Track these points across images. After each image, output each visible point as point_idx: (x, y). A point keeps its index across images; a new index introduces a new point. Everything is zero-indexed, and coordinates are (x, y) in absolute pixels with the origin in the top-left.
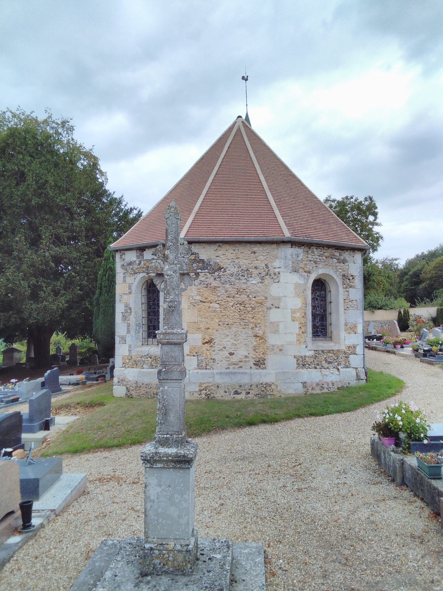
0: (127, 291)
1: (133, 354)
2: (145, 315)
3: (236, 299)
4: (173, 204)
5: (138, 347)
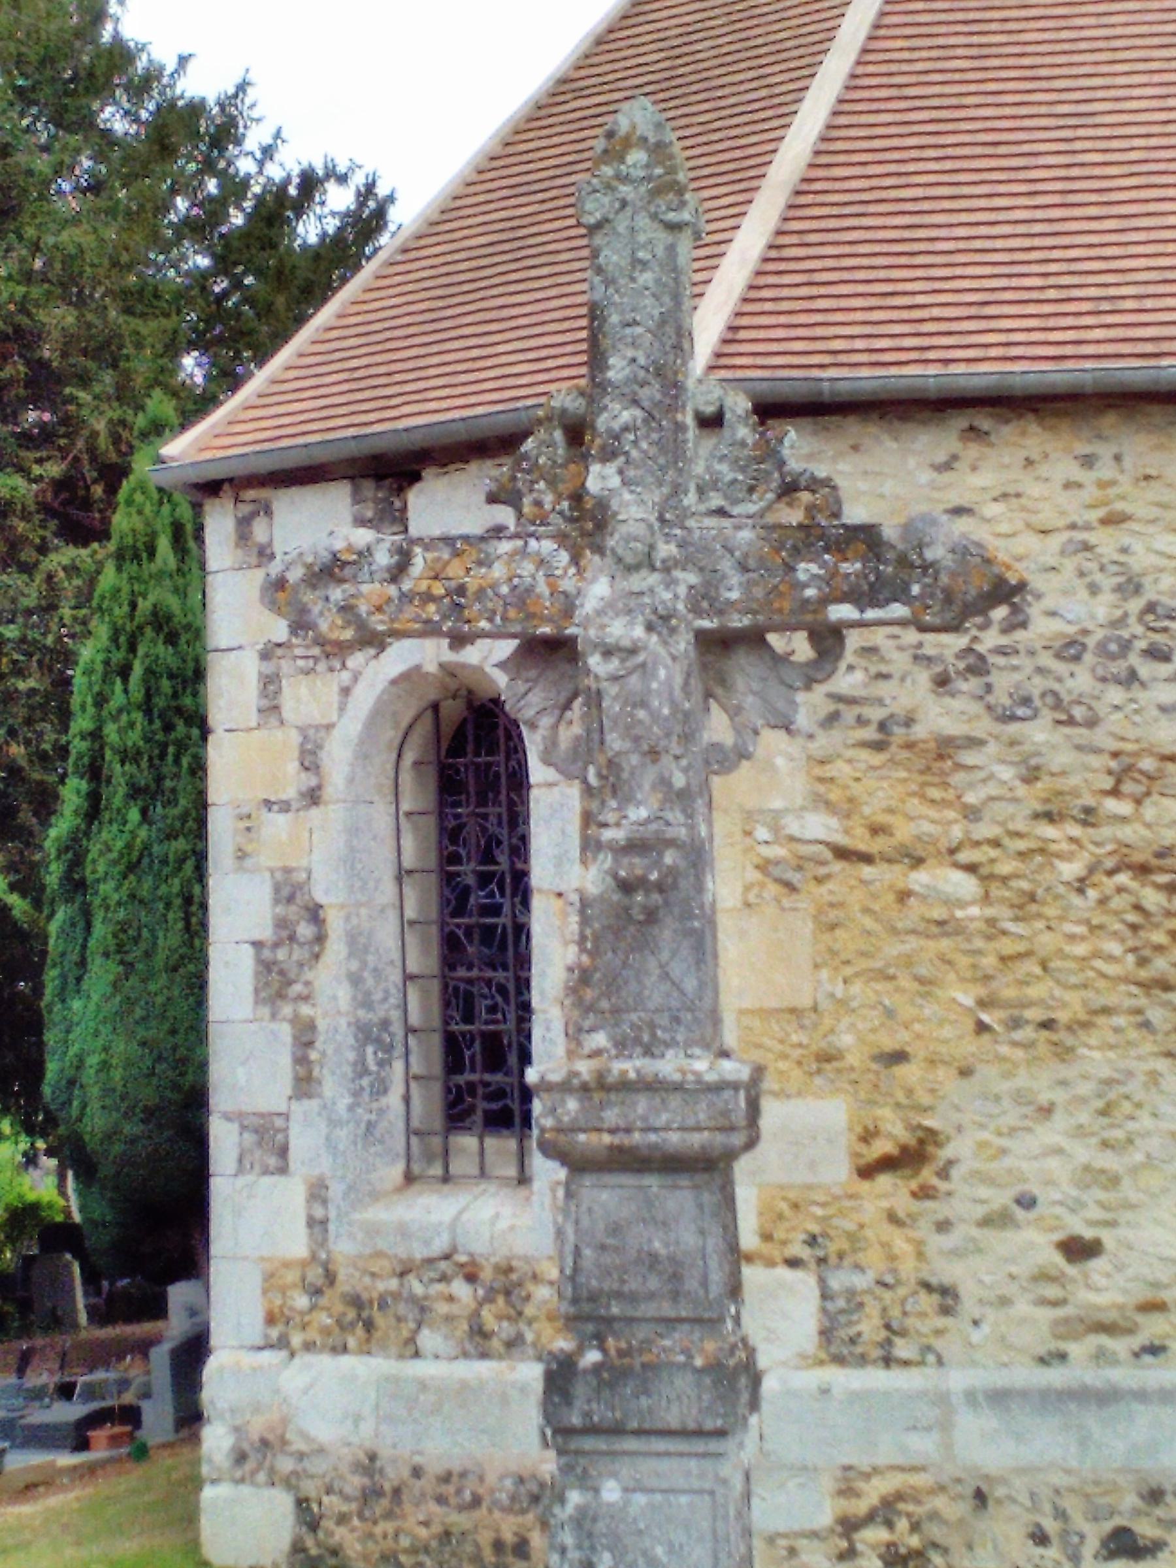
0: (292, 783)
1: (344, 1247)
2: (423, 958)
3: (1106, 832)
4: (637, 116)
5: (375, 1196)
